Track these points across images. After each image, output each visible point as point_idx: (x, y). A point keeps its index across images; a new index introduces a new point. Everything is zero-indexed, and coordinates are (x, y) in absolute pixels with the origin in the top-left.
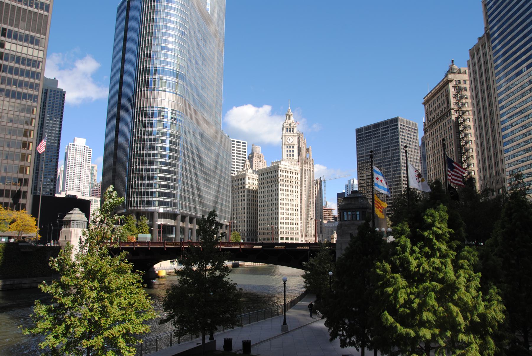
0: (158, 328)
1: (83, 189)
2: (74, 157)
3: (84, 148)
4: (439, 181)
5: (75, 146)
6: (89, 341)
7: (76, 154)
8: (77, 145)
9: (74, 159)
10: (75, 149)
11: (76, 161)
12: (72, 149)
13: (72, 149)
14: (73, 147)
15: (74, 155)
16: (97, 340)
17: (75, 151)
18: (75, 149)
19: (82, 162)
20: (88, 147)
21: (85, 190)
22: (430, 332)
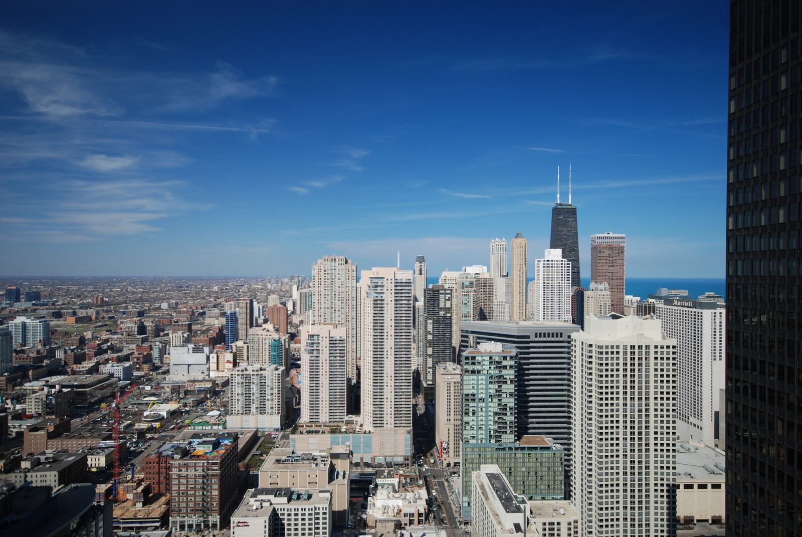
0: (227, 371)
1: (563, 317)
2: (550, 276)
3: (561, 262)
4: (17, 469)
5: (550, 262)
6: (6, 290)
7: (552, 272)
8: (552, 261)
9: (550, 279)
10: (550, 266)
11: (553, 282)
12: (549, 278)
13: (549, 278)
14: (547, 264)
15: (550, 274)
16: (254, 508)
17: (550, 268)
18: (550, 266)
19: (561, 282)
20: (566, 260)
21: (567, 317)
22: (305, 500)
